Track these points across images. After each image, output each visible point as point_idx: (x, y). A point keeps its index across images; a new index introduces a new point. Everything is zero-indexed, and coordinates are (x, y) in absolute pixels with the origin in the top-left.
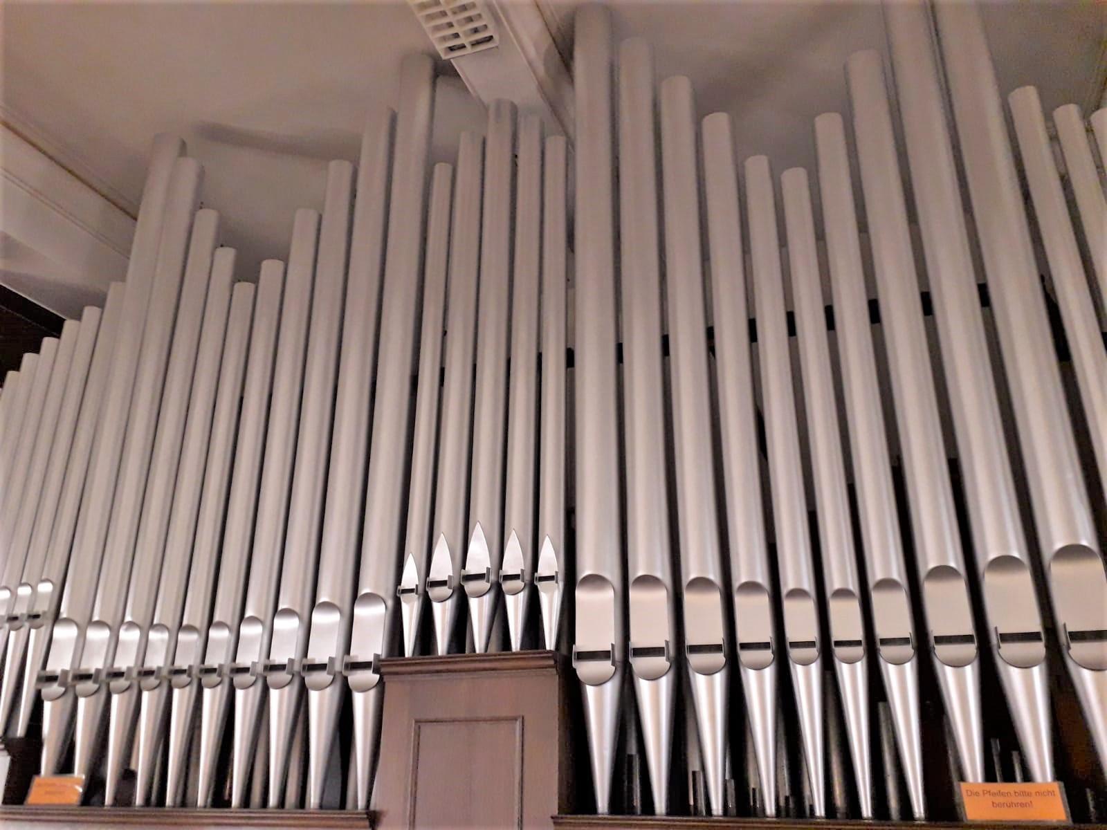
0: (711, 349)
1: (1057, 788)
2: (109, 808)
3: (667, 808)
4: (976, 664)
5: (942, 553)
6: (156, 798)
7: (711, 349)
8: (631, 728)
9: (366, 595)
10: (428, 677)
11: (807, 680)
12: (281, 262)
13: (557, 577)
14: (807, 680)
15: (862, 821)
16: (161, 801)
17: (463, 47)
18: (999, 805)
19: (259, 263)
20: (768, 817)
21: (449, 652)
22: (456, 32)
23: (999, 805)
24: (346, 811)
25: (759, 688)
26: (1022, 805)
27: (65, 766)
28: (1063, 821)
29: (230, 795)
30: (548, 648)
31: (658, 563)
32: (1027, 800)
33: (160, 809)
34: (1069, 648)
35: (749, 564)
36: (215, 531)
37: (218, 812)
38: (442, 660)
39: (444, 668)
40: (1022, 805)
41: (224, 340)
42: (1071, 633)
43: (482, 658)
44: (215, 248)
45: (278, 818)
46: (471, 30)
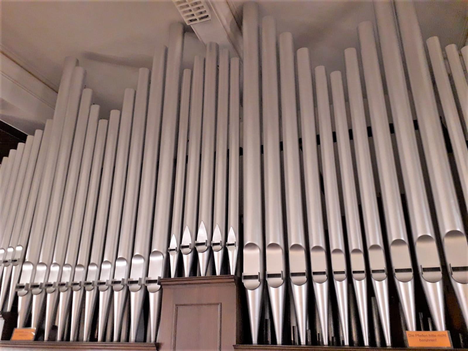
0: (301, 148)
1: (447, 333)
2: (46, 342)
3: (282, 342)
4: (413, 281)
5: (398, 234)
6: (66, 338)
7: (301, 148)
8: (267, 308)
9: (155, 251)
10: (181, 286)
11: (341, 288)
12: (119, 111)
13: (235, 244)
14: (341, 288)
15: (364, 347)
16: (68, 339)
17: (196, 20)
18: (422, 340)
19: (110, 112)
20: (324, 345)
21: (190, 276)
22: (193, 13)
23: (422, 340)
24: (146, 343)
25: (321, 291)
26: (432, 340)
27: (28, 324)
28: (450, 347)
29: (97, 336)
30: (232, 274)
31: (278, 238)
32: (434, 338)
33: (68, 342)
34: (452, 274)
35: (317, 239)
36: (91, 225)
37: (92, 343)
38: (187, 279)
39: (188, 283)
40: (432, 340)
41: (95, 144)
42: (453, 268)
43: (204, 278)
44: (91, 105)
45: (118, 346)
46: (199, 13)
